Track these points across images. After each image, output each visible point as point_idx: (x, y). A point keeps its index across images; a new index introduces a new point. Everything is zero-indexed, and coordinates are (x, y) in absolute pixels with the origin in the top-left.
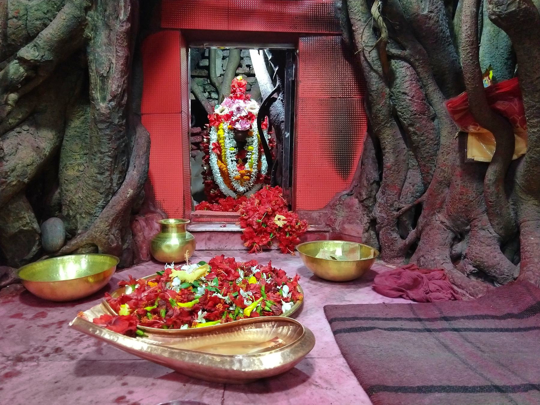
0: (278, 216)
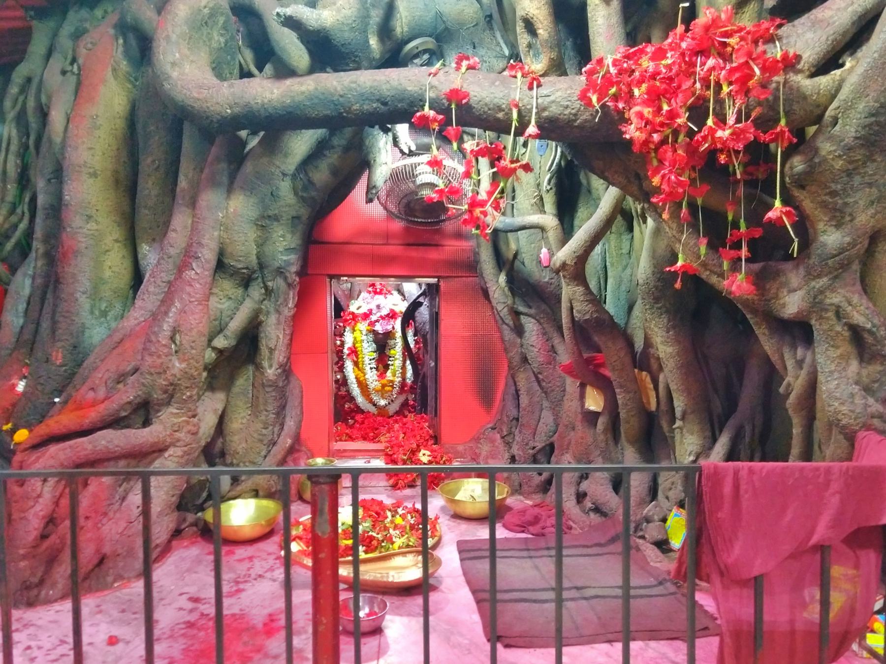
0: (423, 451)
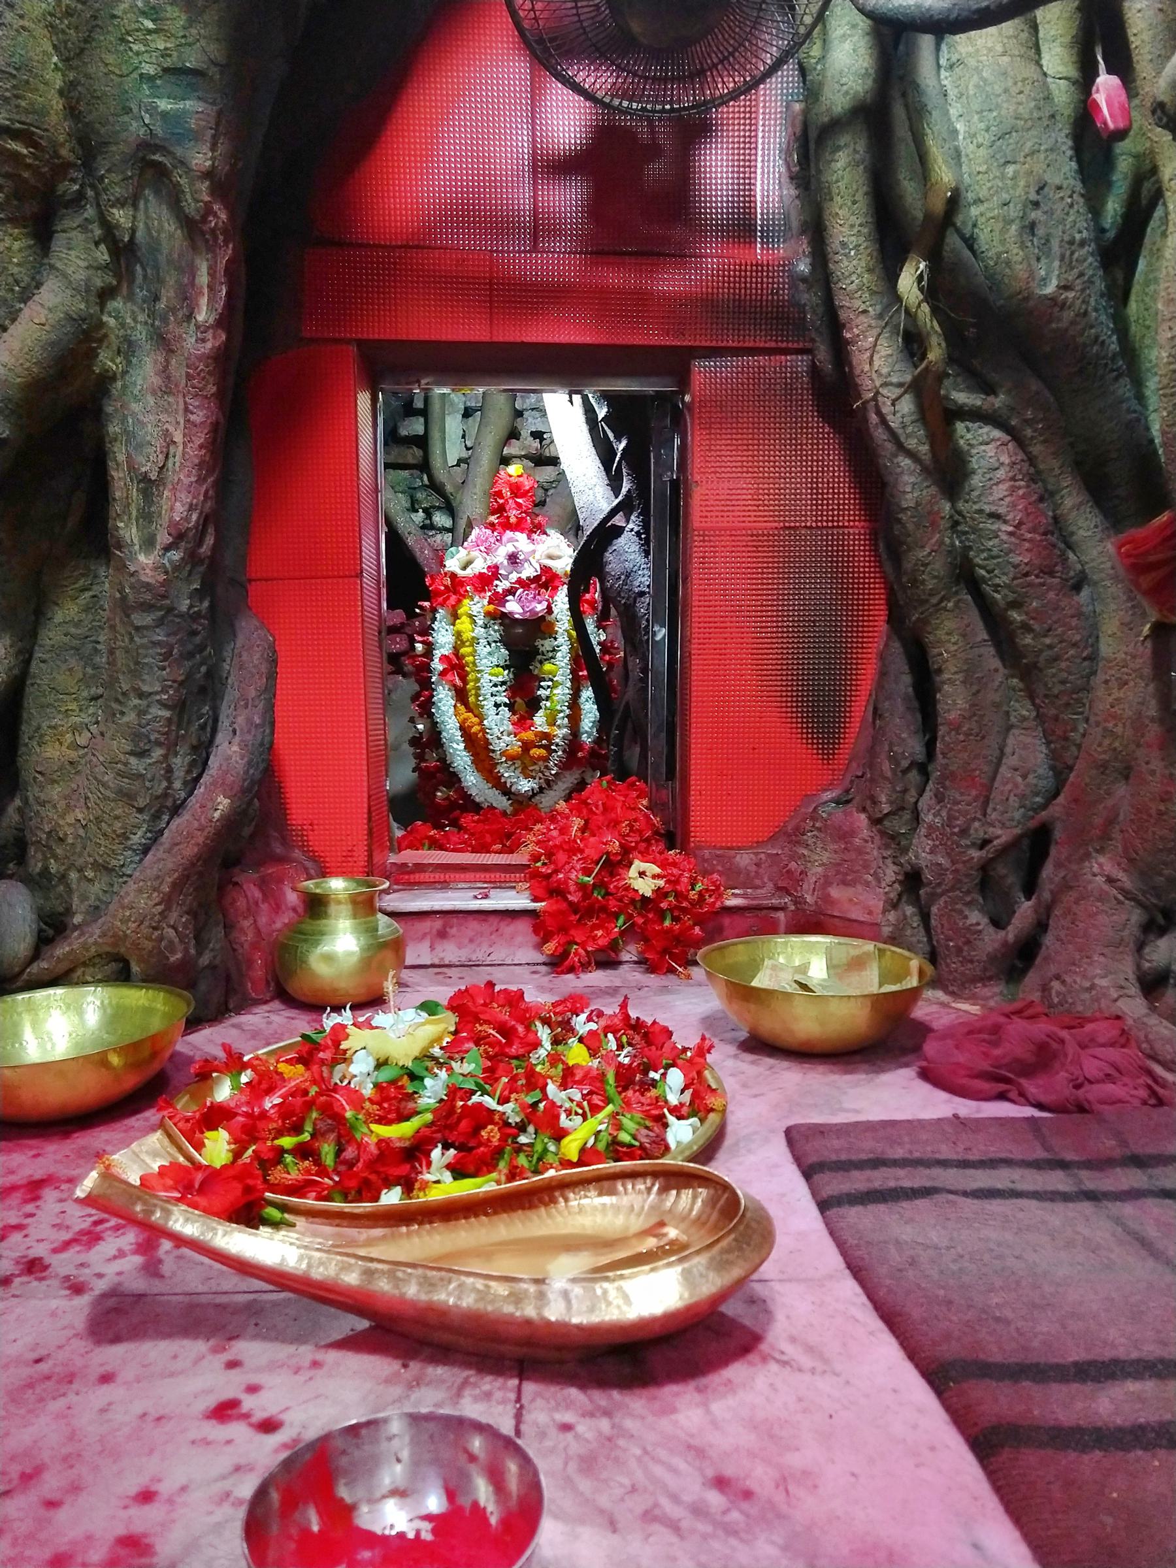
0: (638, 865)
